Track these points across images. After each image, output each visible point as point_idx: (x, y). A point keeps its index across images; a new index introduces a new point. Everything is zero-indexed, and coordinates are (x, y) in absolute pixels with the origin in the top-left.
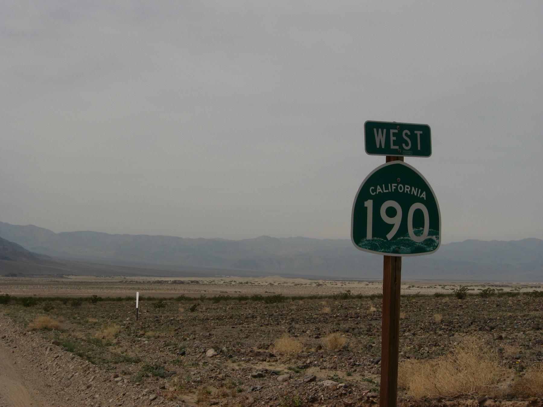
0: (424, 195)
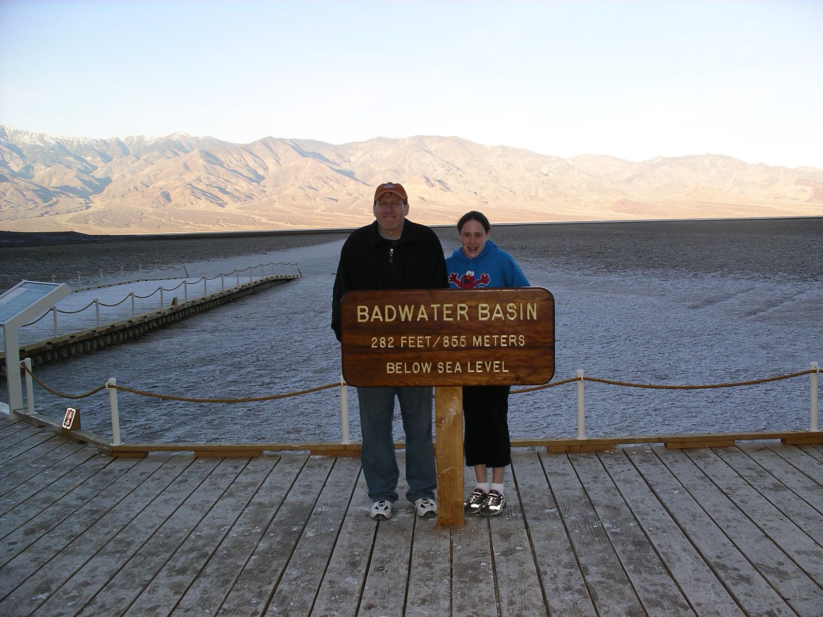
0: (377, 314)
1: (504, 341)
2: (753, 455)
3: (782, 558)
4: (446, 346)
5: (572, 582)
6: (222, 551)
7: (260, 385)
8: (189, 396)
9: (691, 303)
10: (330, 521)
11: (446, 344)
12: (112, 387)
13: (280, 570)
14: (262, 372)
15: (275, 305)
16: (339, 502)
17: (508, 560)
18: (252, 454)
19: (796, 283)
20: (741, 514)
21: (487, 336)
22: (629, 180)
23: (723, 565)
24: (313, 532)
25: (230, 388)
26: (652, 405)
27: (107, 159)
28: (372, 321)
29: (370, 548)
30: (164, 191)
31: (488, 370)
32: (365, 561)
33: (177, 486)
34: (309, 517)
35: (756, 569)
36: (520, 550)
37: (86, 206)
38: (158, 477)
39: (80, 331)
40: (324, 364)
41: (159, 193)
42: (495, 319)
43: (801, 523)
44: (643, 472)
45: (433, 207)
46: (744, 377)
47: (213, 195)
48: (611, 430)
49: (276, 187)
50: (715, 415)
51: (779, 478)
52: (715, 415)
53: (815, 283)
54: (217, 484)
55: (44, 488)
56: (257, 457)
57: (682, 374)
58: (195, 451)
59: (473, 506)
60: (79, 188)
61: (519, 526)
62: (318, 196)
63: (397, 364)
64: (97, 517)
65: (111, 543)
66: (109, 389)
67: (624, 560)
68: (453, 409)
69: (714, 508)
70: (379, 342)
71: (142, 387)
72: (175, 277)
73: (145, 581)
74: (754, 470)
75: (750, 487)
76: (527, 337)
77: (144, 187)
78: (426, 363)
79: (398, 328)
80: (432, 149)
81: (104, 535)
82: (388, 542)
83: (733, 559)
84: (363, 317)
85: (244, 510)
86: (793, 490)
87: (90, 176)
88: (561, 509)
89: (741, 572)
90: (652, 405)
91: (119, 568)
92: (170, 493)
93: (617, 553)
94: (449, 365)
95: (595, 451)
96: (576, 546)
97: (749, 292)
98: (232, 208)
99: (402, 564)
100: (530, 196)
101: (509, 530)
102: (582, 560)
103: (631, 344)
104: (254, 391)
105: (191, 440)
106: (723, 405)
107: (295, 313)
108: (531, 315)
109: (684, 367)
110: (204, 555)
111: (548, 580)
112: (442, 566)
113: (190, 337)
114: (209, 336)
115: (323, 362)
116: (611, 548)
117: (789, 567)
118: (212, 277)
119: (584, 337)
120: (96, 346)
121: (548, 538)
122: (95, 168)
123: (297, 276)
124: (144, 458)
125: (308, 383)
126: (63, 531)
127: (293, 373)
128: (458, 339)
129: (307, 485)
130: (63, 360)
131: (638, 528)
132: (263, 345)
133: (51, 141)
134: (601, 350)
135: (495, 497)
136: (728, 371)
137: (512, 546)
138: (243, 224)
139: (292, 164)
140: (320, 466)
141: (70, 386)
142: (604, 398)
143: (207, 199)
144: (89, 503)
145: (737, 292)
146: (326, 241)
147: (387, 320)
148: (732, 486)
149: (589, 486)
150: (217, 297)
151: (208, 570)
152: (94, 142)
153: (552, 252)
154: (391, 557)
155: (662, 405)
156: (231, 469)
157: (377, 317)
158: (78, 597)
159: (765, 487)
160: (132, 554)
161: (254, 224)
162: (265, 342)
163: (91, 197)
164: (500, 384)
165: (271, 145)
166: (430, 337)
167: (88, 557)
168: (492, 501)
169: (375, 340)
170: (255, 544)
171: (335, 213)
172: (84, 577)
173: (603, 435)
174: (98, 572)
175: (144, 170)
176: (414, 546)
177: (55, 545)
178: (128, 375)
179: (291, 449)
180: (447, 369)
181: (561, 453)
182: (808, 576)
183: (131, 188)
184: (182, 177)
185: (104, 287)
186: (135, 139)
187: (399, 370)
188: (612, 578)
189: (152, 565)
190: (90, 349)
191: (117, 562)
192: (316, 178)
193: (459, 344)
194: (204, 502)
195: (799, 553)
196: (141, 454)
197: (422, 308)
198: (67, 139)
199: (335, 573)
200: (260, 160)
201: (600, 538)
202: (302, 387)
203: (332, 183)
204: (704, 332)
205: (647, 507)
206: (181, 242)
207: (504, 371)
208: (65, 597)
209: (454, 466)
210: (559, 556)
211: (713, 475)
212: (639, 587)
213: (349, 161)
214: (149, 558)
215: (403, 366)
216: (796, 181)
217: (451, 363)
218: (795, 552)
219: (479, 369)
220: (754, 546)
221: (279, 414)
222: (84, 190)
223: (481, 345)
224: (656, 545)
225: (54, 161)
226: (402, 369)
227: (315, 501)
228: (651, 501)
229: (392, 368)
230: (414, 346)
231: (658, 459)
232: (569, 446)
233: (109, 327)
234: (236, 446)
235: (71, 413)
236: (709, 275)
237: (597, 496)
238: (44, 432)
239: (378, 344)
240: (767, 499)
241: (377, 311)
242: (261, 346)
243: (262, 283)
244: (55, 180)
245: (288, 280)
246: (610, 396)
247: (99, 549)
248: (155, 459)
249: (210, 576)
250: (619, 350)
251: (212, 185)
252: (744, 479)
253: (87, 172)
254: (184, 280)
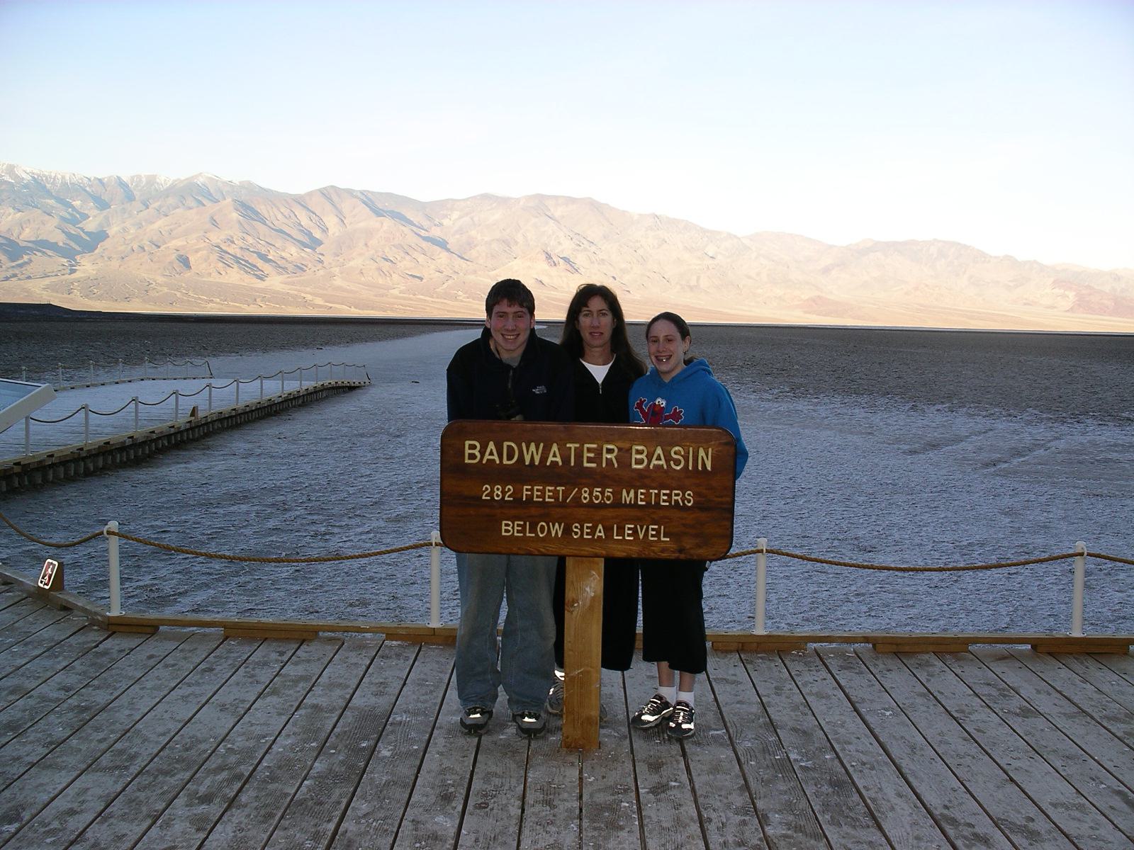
0: (491, 454)
1: (665, 498)
2: (993, 666)
3: (1032, 811)
4: (585, 502)
5: (747, 834)
6: (262, 773)
7: (312, 536)
8: (212, 548)
9: (907, 447)
10: (413, 734)
11: (585, 498)
12: (113, 533)
13: (345, 801)
14: (315, 517)
15: (332, 424)
16: (426, 708)
17: (659, 800)
18: (302, 636)
19: (1051, 425)
20: (976, 747)
21: (642, 491)
22: (826, 270)
23: (951, 818)
24: (389, 751)
25: (271, 539)
26: (853, 588)
27: (103, 205)
28: (484, 462)
29: (468, 776)
30: (181, 254)
31: (641, 537)
32: (462, 794)
33: (199, 676)
34: (384, 727)
35: (997, 825)
36: (674, 786)
37: (71, 270)
38: (172, 662)
39: (60, 448)
40: (401, 510)
41: (174, 256)
42: (653, 467)
43: (1058, 764)
44: (843, 683)
45: (554, 294)
46: (980, 554)
47: (250, 264)
48: (797, 621)
49: (338, 256)
50: (939, 605)
51: (1028, 700)
52: (939, 605)
53: (1076, 425)
54: (255, 676)
55: (11, 673)
56: (311, 641)
57: (894, 545)
58: (225, 627)
59: (644, 718)
60: (61, 244)
61: (674, 753)
62: (395, 271)
63: (516, 523)
64: (86, 717)
65: (108, 755)
66: (108, 536)
67: (818, 807)
68: (590, 587)
69: (940, 738)
70: (492, 491)
71: (147, 531)
72: (194, 377)
73: (155, 811)
74: (994, 686)
75: (989, 710)
76: (696, 494)
77: (154, 246)
78: (557, 524)
79: (520, 474)
80: (557, 214)
81: (96, 743)
82: (493, 769)
83: (966, 810)
84: (472, 456)
85: (293, 714)
86: (1048, 717)
87: (79, 228)
88: (731, 731)
89: (978, 830)
90: (853, 588)
91: (119, 790)
92: (190, 686)
93: (808, 796)
94: (588, 528)
95: (778, 651)
96: (753, 784)
97: (987, 435)
98: (276, 282)
99: (512, 801)
100: (689, 286)
101: (660, 758)
102: (760, 804)
103: (825, 500)
104: (303, 543)
105: (216, 610)
106: (950, 592)
107: (362, 435)
108: (704, 464)
109: (897, 537)
110: (238, 777)
111: (714, 830)
112: (568, 805)
113: (214, 463)
114: (242, 462)
115: (400, 507)
116: (800, 788)
117: (1041, 825)
118: (246, 378)
119: (760, 488)
120: (82, 469)
121: (713, 771)
122: (86, 217)
123: (365, 383)
124: (153, 634)
125: (379, 535)
126: (39, 735)
127: (358, 520)
128: (602, 493)
129: (381, 683)
130: (36, 488)
131: (836, 762)
132: (316, 478)
133: (24, 176)
134: (784, 507)
135: (686, 711)
136: (957, 544)
137: (664, 781)
138: (290, 306)
139: (362, 225)
140: (398, 656)
141: (46, 526)
142: (789, 574)
143: (240, 268)
144: (75, 697)
145: (971, 434)
146: (404, 336)
147: (505, 462)
148: (965, 708)
149: (770, 699)
150: (253, 409)
151: (244, 798)
152: (86, 181)
153: (717, 364)
154: (497, 788)
155: (867, 589)
156: (274, 656)
157: (491, 457)
158: (60, 831)
159: (1009, 712)
160: (136, 772)
161: (305, 306)
162: (318, 475)
163: (78, 258)
164: (657, 556)
165: (335, 198)
166: (563, 488)
167: (75, 774)
168: (683, 717)
169: (487, 489)
170: (309, 763)
171: (418, 297)
172: (69, 802)
173: (786, 626)
174: (88, 797)
175: (154, 223)
176: (528, 775)
177: (27, 755)
178: (127, 513)
179: (359, 630)
180: (585, 533)
181: (731, 652)
182: (1068, 838)
183: (135, 247)
184: (207, 235)
185: (95, 385)
186: (144, 179)
187: (518, 531)
188: (801, 832)
189: (165, 788)
190: (75, 473)
191: (116, 782)
192: (394, 245)
193: (603, 499)
194: (237, 701)
195: (1055, 805)
196: (148, 629)
197: (555, 448)
198: (47, 174)
199: (421, 809)
200: (317, 218)
201: (784, 775)
202: (370, 541)
203: (415, 255)
204: (925, 488)
205: (849, 733)
206: (208, 327)
207: (663, 539)
208: (43, 830)
209: (587, 666)
210: (729, 797)
211: (939, 692)
212: (838, 845)
213: (441, 224)
214: (161, 778)
215: (524, 527)
216: (1055, 282)
217: (590, 525)
218: (1050, 804)
219: (629, 535)
220: (994, 794)
221: (338, 579)
222: (67, 247)
223: (633, 502)
224: (860, 786)
225: (28, 204)
226: (523, 531)
227: (391, 706)
228: (854, 724)
229: (509, 528)
230: (541, 500)
231: (863, 666)
232: (743, 643)
233: (102, 444)
234: (281, 623)
235: (51, 566)
236: (933, 409)
237: (780, 714)
238: (11, 592)
239: (491, 494)
240: (1012, 728)
241: (491, 450)
242: (313, 480)
243: (316, 391)
244: (27, 230)
245: (352, 388)
246: (796, 572)
247: (90, 762)
248: (167, 637)
249: (246, 806)
250: (808, 508)
251: (248, 249)
252: (982, 700)
253: (74, 222)
254: (207, 381)
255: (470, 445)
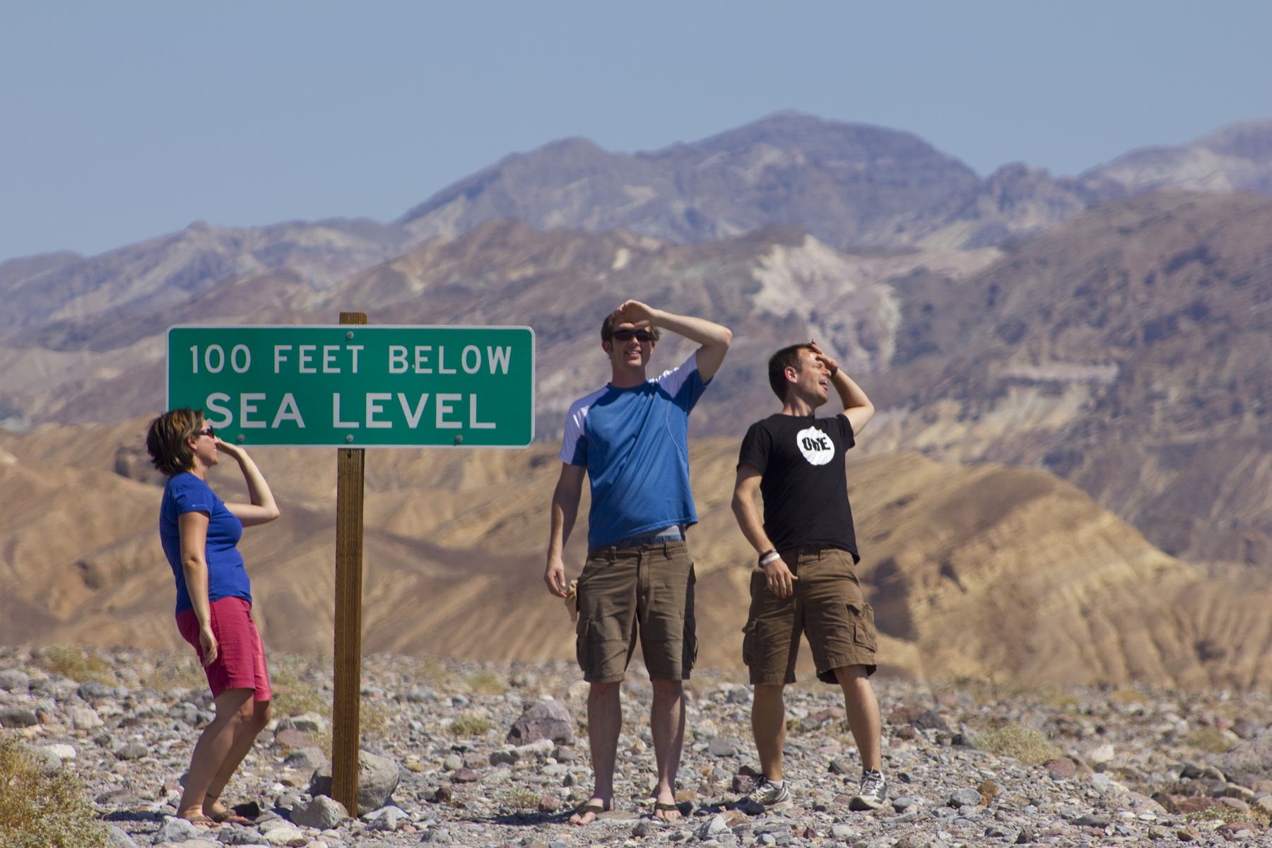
0: (289, 410)
187: (423, 365)
215: (433, 357)
226: (432, 363)
255: (395, 351)
